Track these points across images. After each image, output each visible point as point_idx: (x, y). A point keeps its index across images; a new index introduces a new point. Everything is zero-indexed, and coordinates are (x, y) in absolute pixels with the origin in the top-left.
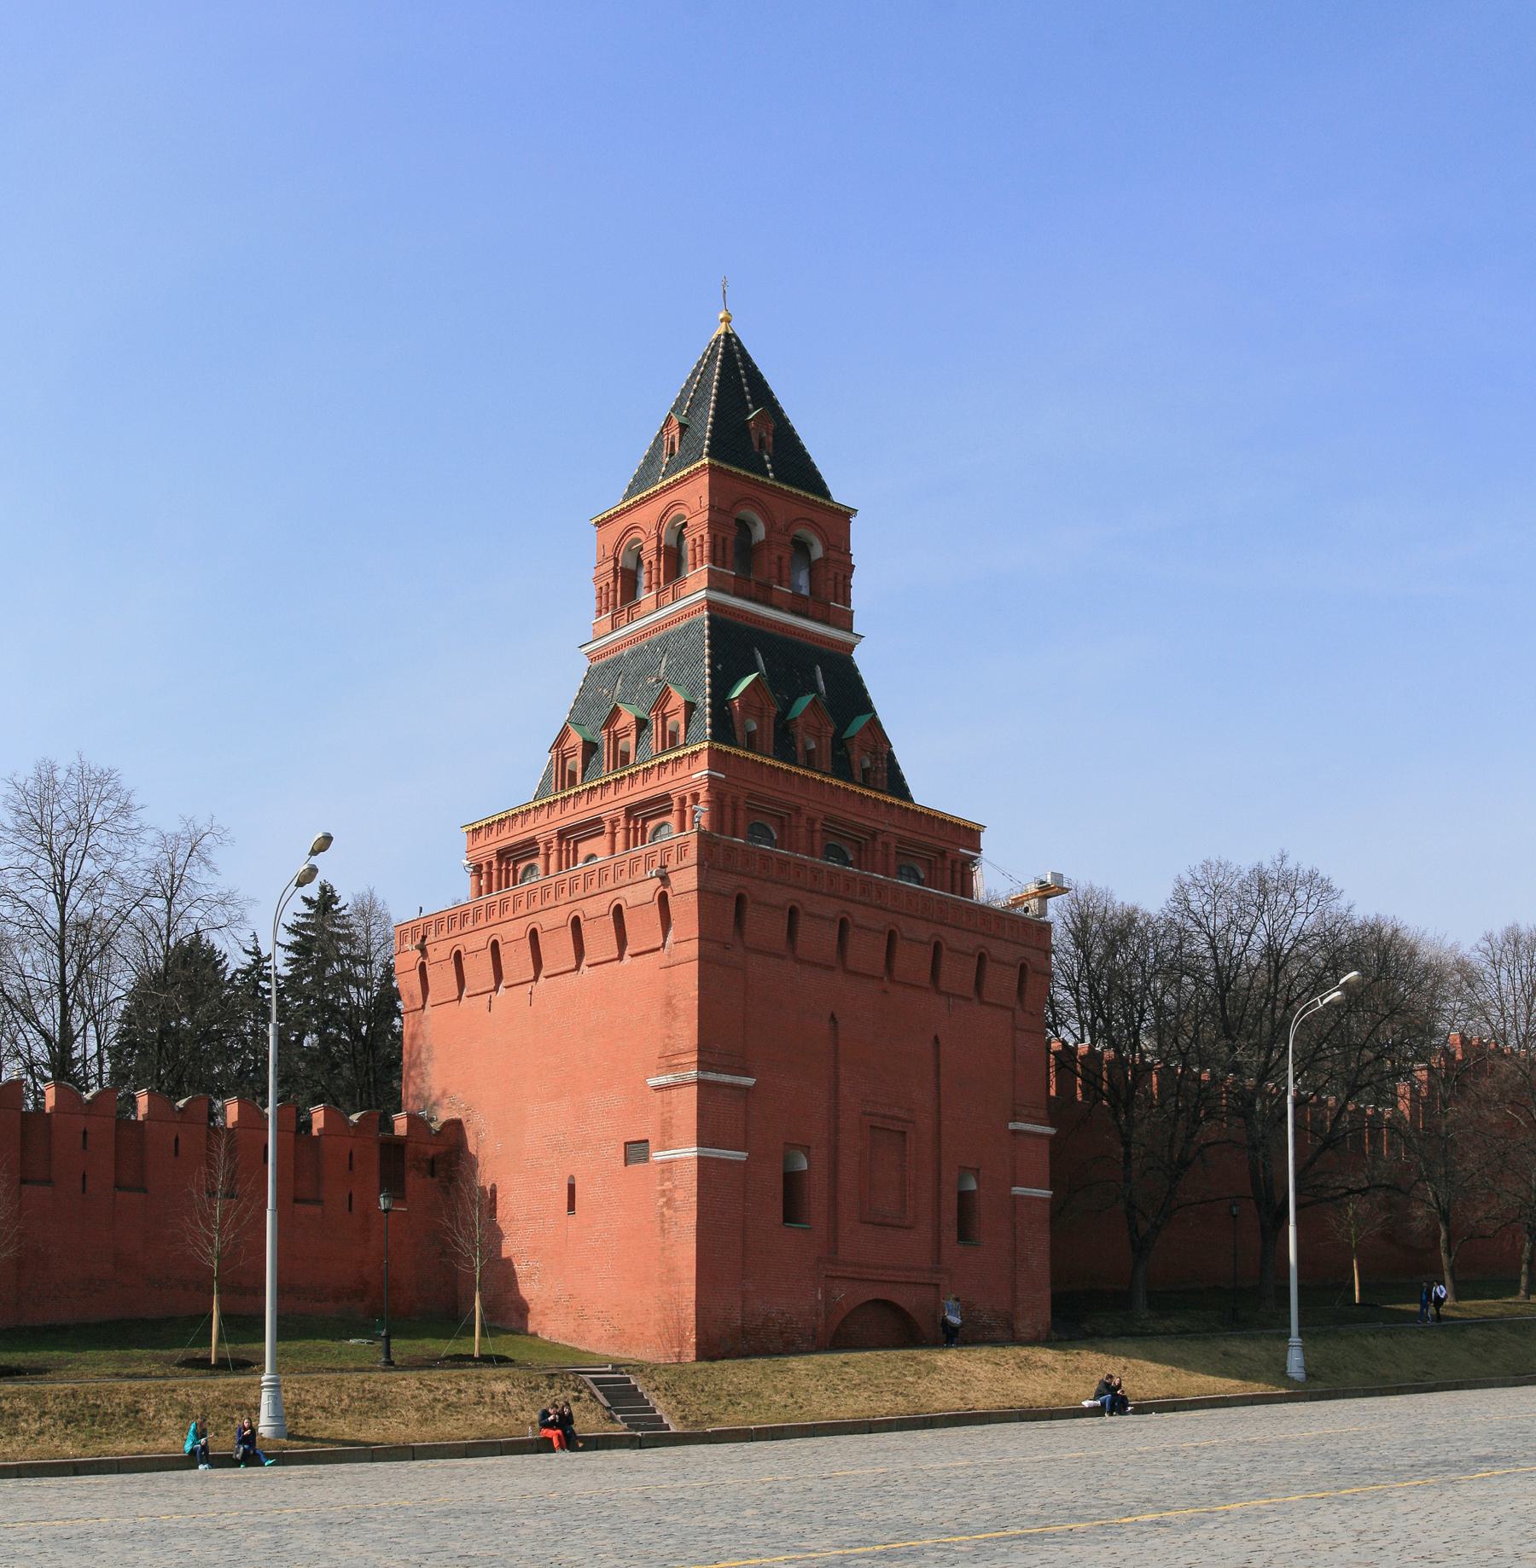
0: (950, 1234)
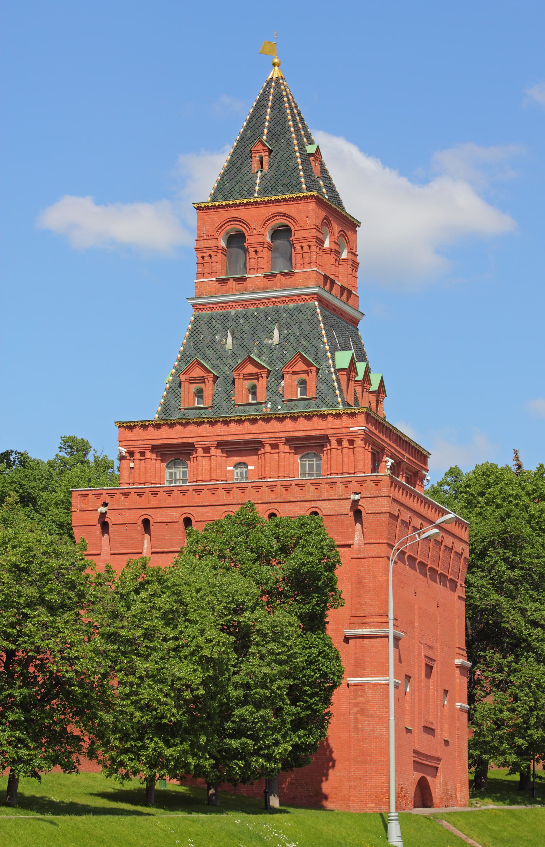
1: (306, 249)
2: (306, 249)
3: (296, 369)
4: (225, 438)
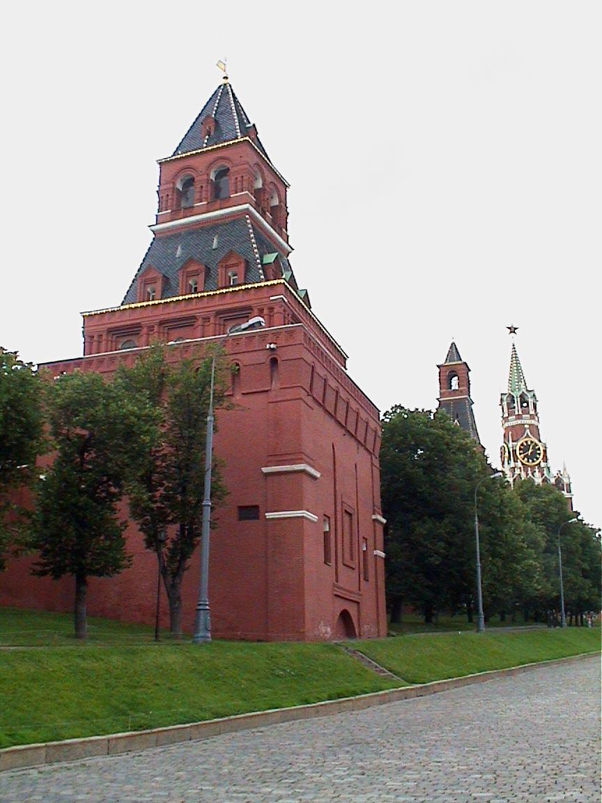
0: (362, 579)
1: (239, 179)
2: (239, 179)
3: (230, 263)
4: (167, 317)
